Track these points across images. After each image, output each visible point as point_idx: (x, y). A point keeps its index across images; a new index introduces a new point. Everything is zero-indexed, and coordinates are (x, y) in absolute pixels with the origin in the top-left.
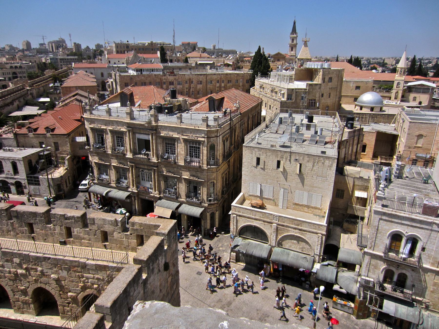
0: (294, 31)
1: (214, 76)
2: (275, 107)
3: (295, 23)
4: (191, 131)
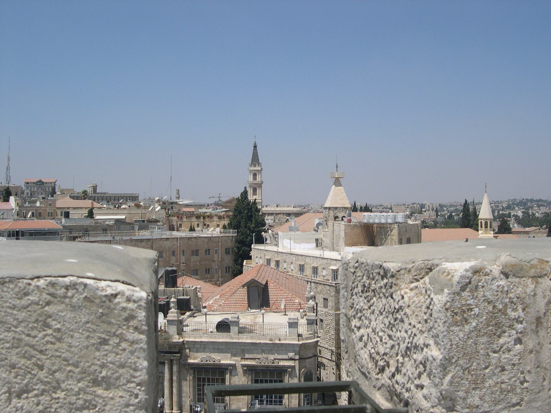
0: (255, 160)
1: (166, 242)
2: (321, 296)
3: (255, 147)
4: (264, 348)
